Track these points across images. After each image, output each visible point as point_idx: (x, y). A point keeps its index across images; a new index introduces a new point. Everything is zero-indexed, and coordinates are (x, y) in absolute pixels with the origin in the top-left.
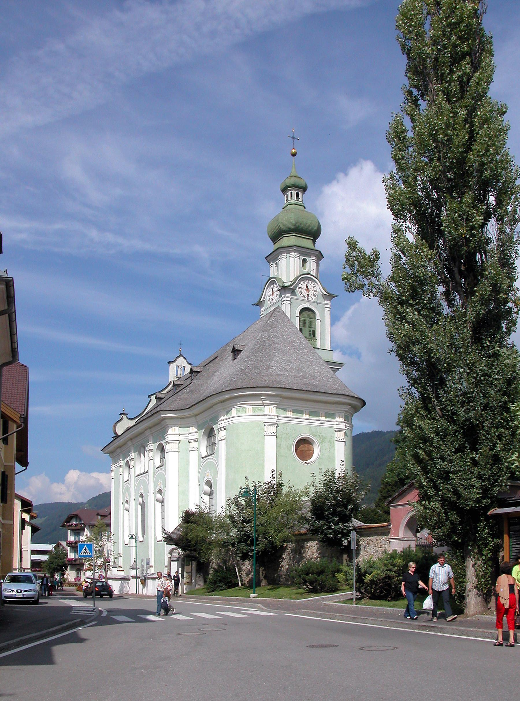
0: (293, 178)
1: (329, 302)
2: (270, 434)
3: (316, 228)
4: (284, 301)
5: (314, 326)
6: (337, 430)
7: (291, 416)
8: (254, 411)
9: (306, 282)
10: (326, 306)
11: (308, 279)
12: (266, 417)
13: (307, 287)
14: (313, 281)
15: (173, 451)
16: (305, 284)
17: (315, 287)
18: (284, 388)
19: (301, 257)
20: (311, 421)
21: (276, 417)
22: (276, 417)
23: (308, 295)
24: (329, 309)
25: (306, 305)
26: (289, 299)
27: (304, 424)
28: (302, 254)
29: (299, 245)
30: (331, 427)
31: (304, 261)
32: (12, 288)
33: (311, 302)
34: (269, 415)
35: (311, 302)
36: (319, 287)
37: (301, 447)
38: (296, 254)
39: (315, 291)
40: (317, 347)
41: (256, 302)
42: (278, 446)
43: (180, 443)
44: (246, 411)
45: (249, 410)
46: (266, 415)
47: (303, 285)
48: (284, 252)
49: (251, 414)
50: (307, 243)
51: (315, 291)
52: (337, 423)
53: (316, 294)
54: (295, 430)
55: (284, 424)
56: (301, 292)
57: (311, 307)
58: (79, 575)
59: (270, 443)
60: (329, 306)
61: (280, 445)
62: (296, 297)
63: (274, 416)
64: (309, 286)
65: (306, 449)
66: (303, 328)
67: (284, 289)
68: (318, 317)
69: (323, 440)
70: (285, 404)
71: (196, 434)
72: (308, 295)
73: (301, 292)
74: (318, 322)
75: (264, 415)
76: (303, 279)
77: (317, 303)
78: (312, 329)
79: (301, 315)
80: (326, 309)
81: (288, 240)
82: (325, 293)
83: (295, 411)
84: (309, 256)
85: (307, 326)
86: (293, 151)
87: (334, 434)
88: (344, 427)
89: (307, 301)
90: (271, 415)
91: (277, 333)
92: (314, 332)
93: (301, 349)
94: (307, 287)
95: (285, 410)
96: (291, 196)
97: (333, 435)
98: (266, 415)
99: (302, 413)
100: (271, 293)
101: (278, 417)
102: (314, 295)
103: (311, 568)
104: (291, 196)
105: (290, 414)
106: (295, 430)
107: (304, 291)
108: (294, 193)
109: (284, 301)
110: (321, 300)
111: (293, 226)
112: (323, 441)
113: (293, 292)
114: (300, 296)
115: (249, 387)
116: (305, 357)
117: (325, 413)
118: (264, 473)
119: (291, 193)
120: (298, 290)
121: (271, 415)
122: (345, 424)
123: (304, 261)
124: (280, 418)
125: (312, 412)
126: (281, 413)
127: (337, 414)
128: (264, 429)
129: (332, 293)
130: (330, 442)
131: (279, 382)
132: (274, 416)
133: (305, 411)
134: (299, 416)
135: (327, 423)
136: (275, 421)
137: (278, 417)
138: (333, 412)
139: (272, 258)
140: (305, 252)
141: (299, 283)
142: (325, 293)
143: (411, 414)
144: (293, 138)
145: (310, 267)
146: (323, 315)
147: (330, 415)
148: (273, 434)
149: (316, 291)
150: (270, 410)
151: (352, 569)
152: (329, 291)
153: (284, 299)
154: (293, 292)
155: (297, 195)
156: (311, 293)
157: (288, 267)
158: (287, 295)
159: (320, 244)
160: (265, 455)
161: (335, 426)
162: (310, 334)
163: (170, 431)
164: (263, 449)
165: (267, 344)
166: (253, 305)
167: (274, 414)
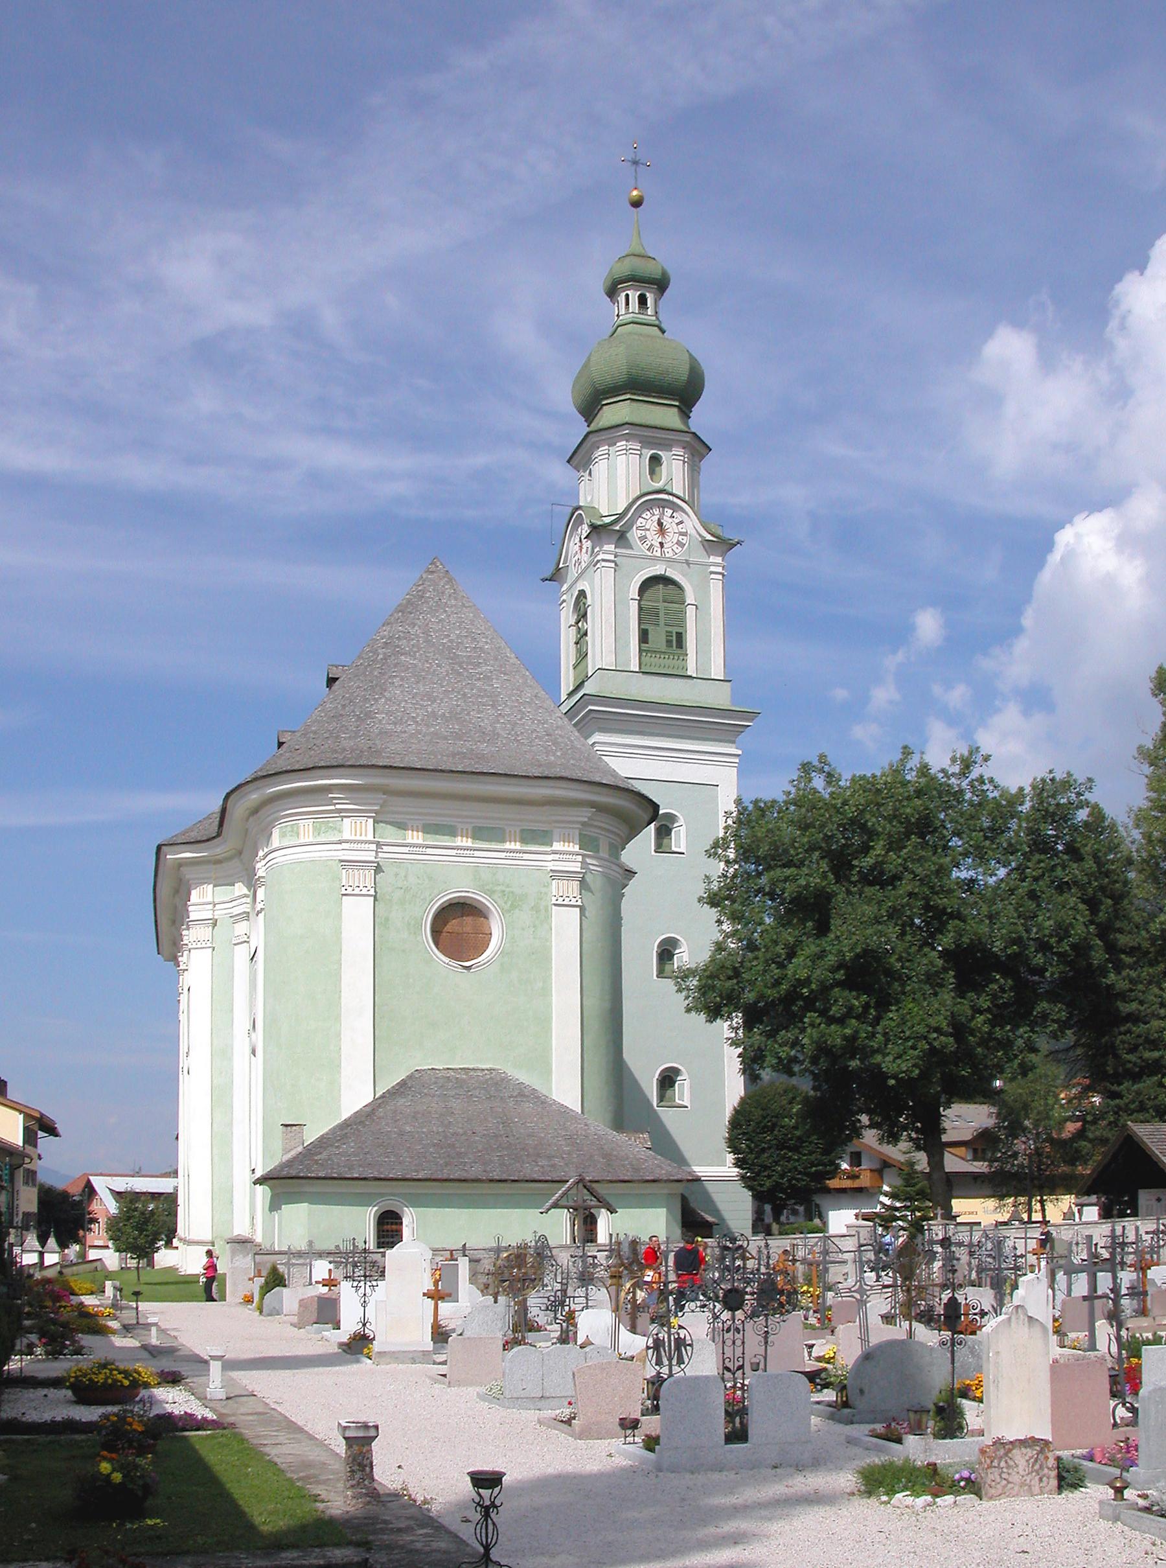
0: (627, 260)
1: (719, 560)
2: (357, 891)
3: (685, 378)
4: (598, 561)
5: (682, 622)
6: (556, 875)
7: (420, 841)
8: (317, 831)
9: (656, 511)
10: (712, 569)
11: (663, 504)
12: (345, 846)
13: (660, 524)
14: (675, 508)
15: (199, 946)
16: (656, 518)
17: (681, 522)
18: (385, 767)
19: (644, 451)
20: (477, 853)
21: (373, 847)
22: (373, 847)
23: (661, 544)
24: (720, 577)
25: (658, 570)
26: (612, 557)
27: (456, 863)
28: (646, 443)
29: (643, 422)
30: (539, 869)
31: (655, 460)
33: (670, 561)
34: (354, 842)
35: (670, 561)
36: (692, 524)
37: (453, 925)
38: (630, 445)
39: (681, 534)
40: (689, 673)
41: (548, 575)
42: (379, 923)
43: (215, 924)
44: (298, 834)
45: (306, 828)
46: (347, 841)
47: (649, 520)
49: (311, 840)
50: (668, 416)
51: (681, 534)
52: (556, 857)
53: (684, 540)
54: (430, 878)
55: (399, 863)
56: (643, 539)
57: (671, 573)
59: (357, 915)
60: (720, 570)
61: (387, 919)
62: (629, 552)
63: (366, 842)
64: (666, 521)
65: (468, 929)
66: (650, 628)
67: (598, 531)
68: (690, 598)
69: (514, 902)
70: (400, 809)
71: (244, 900)
74: (690, 612)
75: (340, 842)
76: (648, 506)
77: (688, 563)
78: (675, 630)
79: (647, 595)
80: (713, 576)
81: (614, 413)
83: (428, 829)
84: (667, 446)
85: (662, 622)
86: (635, 193)
87: (548, 886)
88: (576, 867)
89: (663, 559)
90: (362, 842)
91: (414, 625)
93: (472, 664)
94: (660, 524)
95: (402, 826)
96: (627, 303)
97: (544, 890)
98: (347, 841)
99: (452, 832)
100: (577, 548)
101: (378, 844)
102: (678, 543)
103: (619, 1243)
104: (627, 303)
105: (415, 837)
106: (430, 878)
107: (654, 538)
108: (634, 296)
109: (598, 561)
110: (699, 556)
111: (623, 378)
112: (513, 907)
113: (621, 538)
114: (641, 548)
115: (296, 767)
116: (479, 684)
117: (522, 831)
118: (340, 998)
119: (627, 295)
120: (634, 535)
121: (362, 842)
122: (580, 858)
123: (655, 460)
124: (385, 849)
125: (480, 828)
126: (390, 834)
127: (556, 832)
128: (340, 880)
129: (727, 534)
130: (536, 909)
131: (378, 753)
132: (366, 842)
133: (460, 826)
134: (446, 841)
135: (526, 856)
136: (370, 856)
137: (378, 844)
138: (545, 827)
139: (580, 458)
140: (653, 438)
141: (638, 514)
143: (961, 839)
144: (635, 163)
145: (670, 473)
146: (703, 589)
147: (536, 836)
148: (364, 891)
149: (685, 534)
150: (357, 829)
152: (719, 532)
153: (599, 558)
154: (621, 538)
155: (642, 300)
156: (671, 538)
157: (614, 479)
158: (606, 547)
159: (703, 417)
160: (344, 948)
161: (551, 866)
162: (669, 642)
163: (195, 896)
164: (338, 932)
165: (381, 656)
166: (544, 580)
167: (370, 837)
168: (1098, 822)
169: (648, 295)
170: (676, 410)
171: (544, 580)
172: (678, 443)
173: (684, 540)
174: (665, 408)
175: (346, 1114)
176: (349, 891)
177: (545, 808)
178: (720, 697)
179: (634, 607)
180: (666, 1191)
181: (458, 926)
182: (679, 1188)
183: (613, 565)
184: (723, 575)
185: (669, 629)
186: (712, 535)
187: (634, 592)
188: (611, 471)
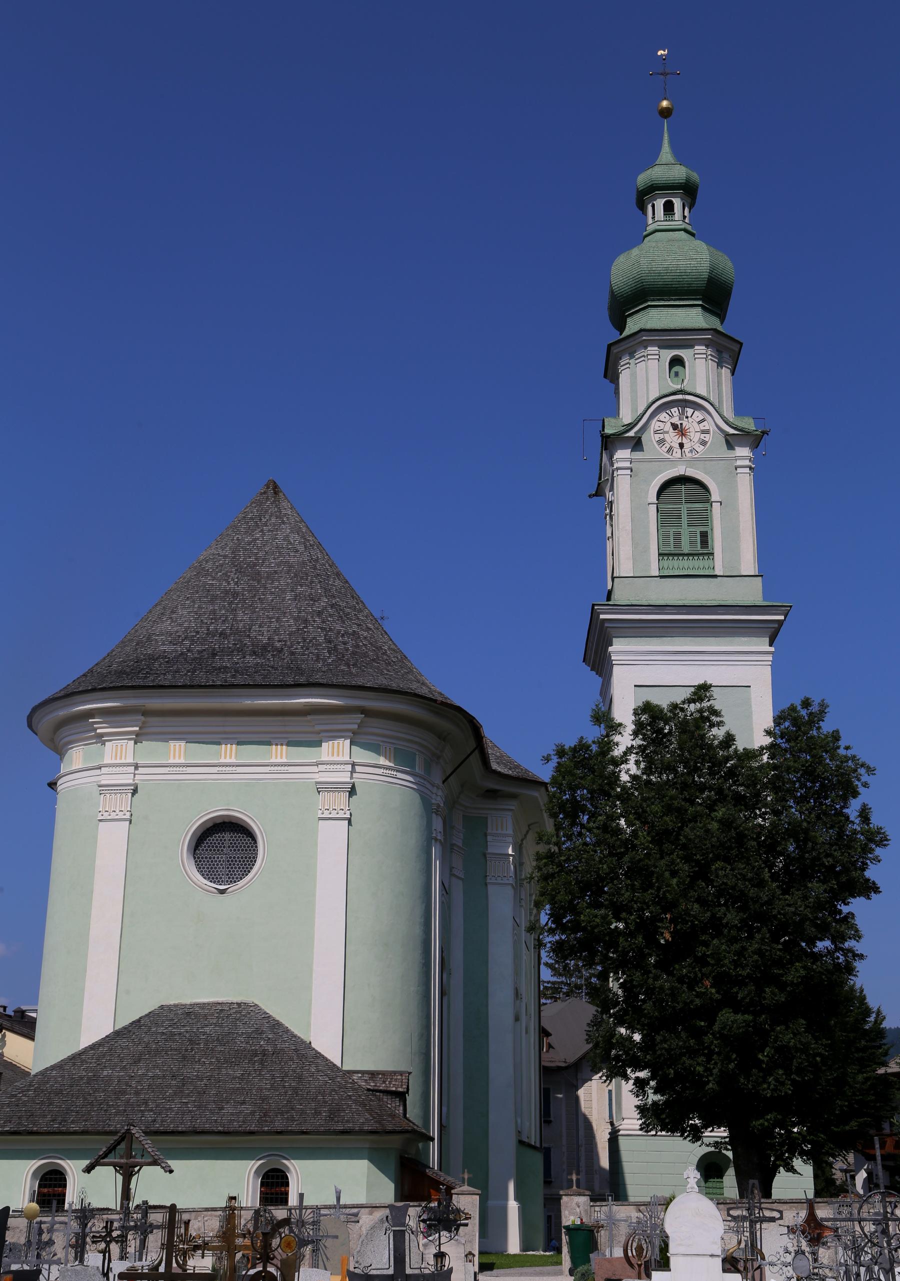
2: (113, 816)
3: (705, 275)
6: (321, 787)
10: (739, 463)
11: (685, 404)
20: (239, 770)
23: (681, 446)
26: (628, 464)
28: (664, 345)
33: (692, 462)
53: (707, 437)
56: (661, 442)
57: (691, 472)
58: (519, 1121)
60: (747, 463)
68: (715, 497)
73: (661, 442)
75: (317, 764)
82: (732, 431)
84: (689, 345)
89: (681, 460)
101: (136, 767)
108: (660, 203)
113: (637, 444)
120: (650, 439)
124: (358, 768)
137: (353, 765)
142: (732, 431)
148: (121, 816)
151: (613, 1221)
155: (669, 208)
156: (693, 439)
166: (590, 496)
170: (700, 309)
173: (707, 437)
174: (688, 309)
175: (87, 1039)
176: (106, 816)
177: (309, 718)
180: (367, 1146)
181: (224, 845)
182: (396, 1141)
184: (751, 468)
186: (735, 429)
187: (652, 497)
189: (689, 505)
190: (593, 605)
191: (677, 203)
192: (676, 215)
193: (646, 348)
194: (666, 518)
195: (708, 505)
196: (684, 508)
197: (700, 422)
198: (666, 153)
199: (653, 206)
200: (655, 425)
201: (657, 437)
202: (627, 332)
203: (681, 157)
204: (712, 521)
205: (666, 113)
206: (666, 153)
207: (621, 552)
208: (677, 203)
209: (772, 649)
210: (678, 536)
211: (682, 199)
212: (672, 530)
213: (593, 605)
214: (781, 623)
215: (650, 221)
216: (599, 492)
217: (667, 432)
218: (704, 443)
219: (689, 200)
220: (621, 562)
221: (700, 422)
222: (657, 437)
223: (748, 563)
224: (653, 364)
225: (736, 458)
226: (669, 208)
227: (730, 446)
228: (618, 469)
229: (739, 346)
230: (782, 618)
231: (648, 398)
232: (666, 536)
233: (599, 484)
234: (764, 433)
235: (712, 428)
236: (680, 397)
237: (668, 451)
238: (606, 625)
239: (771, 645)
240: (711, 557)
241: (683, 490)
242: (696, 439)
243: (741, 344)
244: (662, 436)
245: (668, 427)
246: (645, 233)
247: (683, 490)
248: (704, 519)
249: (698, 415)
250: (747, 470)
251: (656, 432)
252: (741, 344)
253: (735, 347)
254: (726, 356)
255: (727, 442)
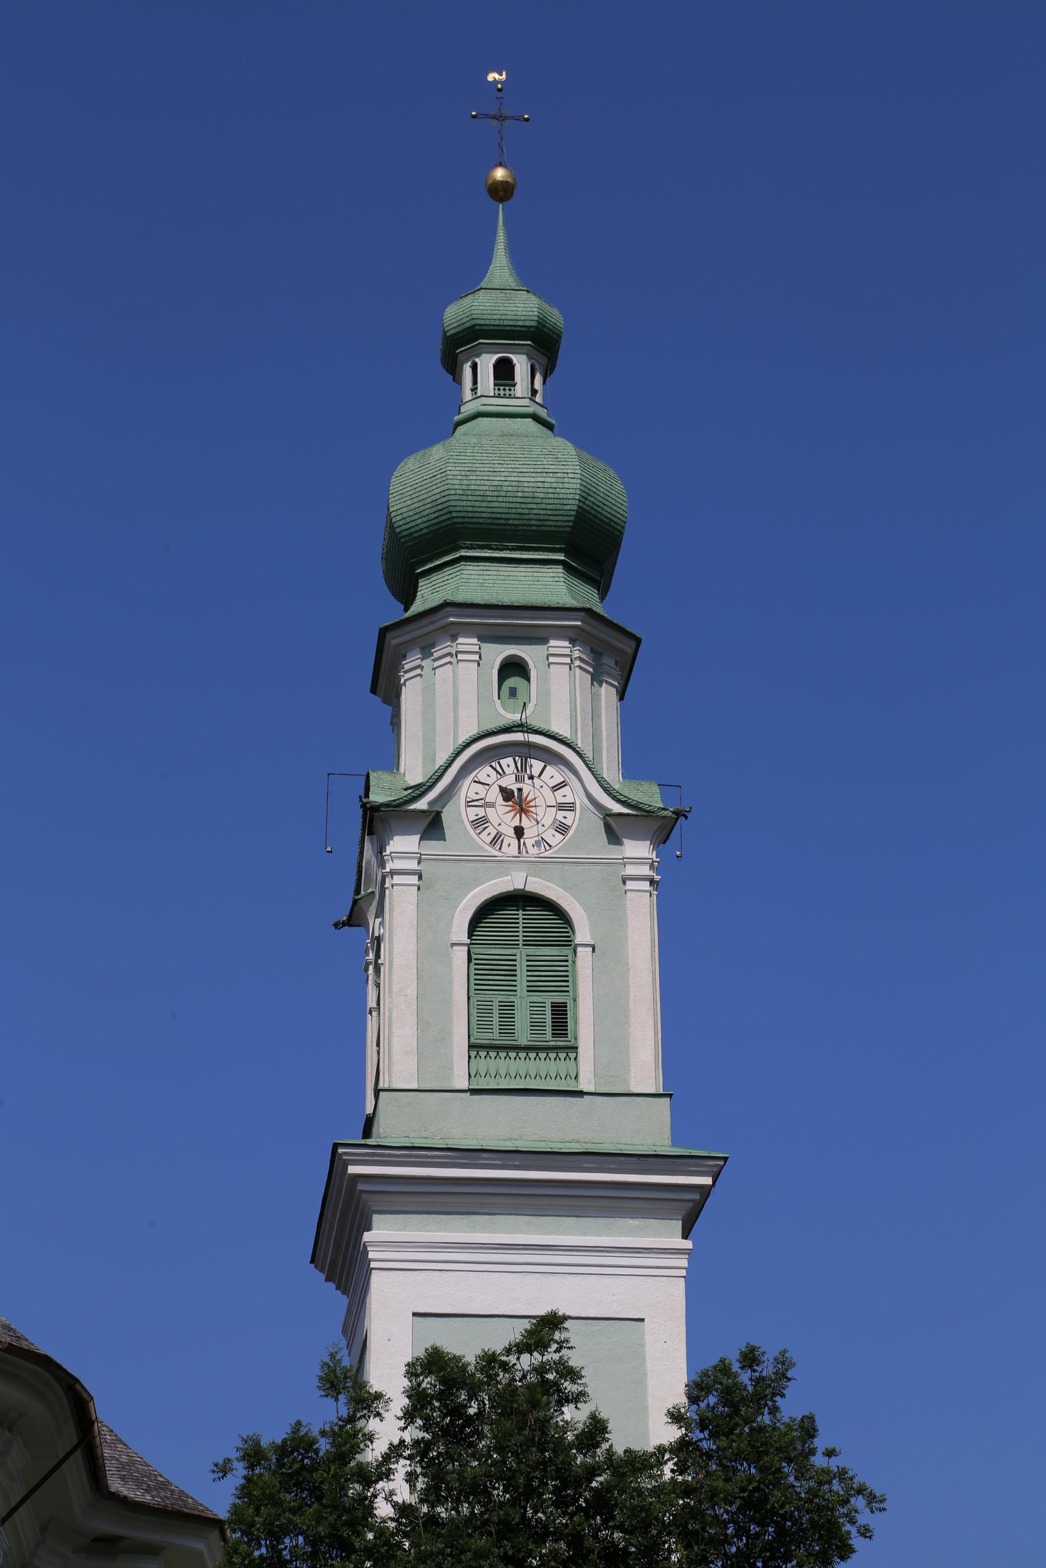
3: (573, 505)
10: (630, 870)
11: (526, 751)
14: (551, 758)
23: (519, 832)
26: (413, 865)
31: (513, 669)
32: (371, 1023)
33: (539, 865)
39: (562, 807)
47: (487, 782)
48: (467, 629)
50: (547, 584)
51: (562, 807)
53: (569, 818)
56: (480, 823)
57: (537, 886)
60: (645, 871)
68: (582, 934)
72: (519, 832)
73: (480, 823)
82: (617, 808)
84: (538, 637)
92: (561, 1015)
108: (487, 363)
113: (432, 826)
120: (457, 816)
123: (513, 669)
142: (617, 808)
149: (569, 807)
154: (432, 826)
155: (504, 372)
166: (336, 925)
168: (465, 1366)
169: (515, 358)
170: (559, 569)
171: (336, 925)
172: (560, 633)
173: (569, 818)
178: (650, 1128)
179: (460, 954)
183: (414, 880)
184: (652, 882)
185: (536, 998)
186: (623, 803)
187: (460, 932)
188: (429, 692)
189: (532, 950)
190: (336, 1146)
191: (521, 364)
192: (518, 387)
193: (454, 638)
194: (486, 975)
195: (567, 951)
196: (522, 955)
197: (555, 788)
198: (500, 268)
199: (474, 367)
200: (468, 789)
201: (473, 813)
202: (417, 607)
203: (529, 275)
204: (575, 984)
205: (501, 192)
206: (500, 268)
207: (395, 1040)
208: (521, 364)
209: (688, 1244)
210: (507, 1011)
211: (530, 357)
212: (497, 998)
213: (336, 1146)
214: (705, 1191)
215: (468, 395)
216: (355, 919)
217: (492, 805)
218: (562, 829)
219: (544, 360)
220: (396, 1058)
221: (555, 788)
222: (473, 813)
223: (645, 1071)
224: (468, 671)
225: (625, 861)
226: (504, 372)
227: (614, 837)
228: (393, 873)
229: (633, 644)
230: (708, 1181)
231: (456, 737)
232: (485, 1010)
233: (355, 902)
234: (679, 814)
235: (581, 800)
236: (518, 737)
237: (493, 842)
238: (361, 1187)
239: (685, 1236)
240: (572, 1055)
241: (519, 920)
242: (548, 821)
243: (638, 641)
244: (481, 812)
245: (494, 795)
246: (457, 418)
247: (519, 920)
248: (562, 978)
249: (553, 774)
250: (646, 886)
251: (469, 804)
252: (638, 641)
253: (628, 647)
254: (608, 661)
255: (609, 830)
